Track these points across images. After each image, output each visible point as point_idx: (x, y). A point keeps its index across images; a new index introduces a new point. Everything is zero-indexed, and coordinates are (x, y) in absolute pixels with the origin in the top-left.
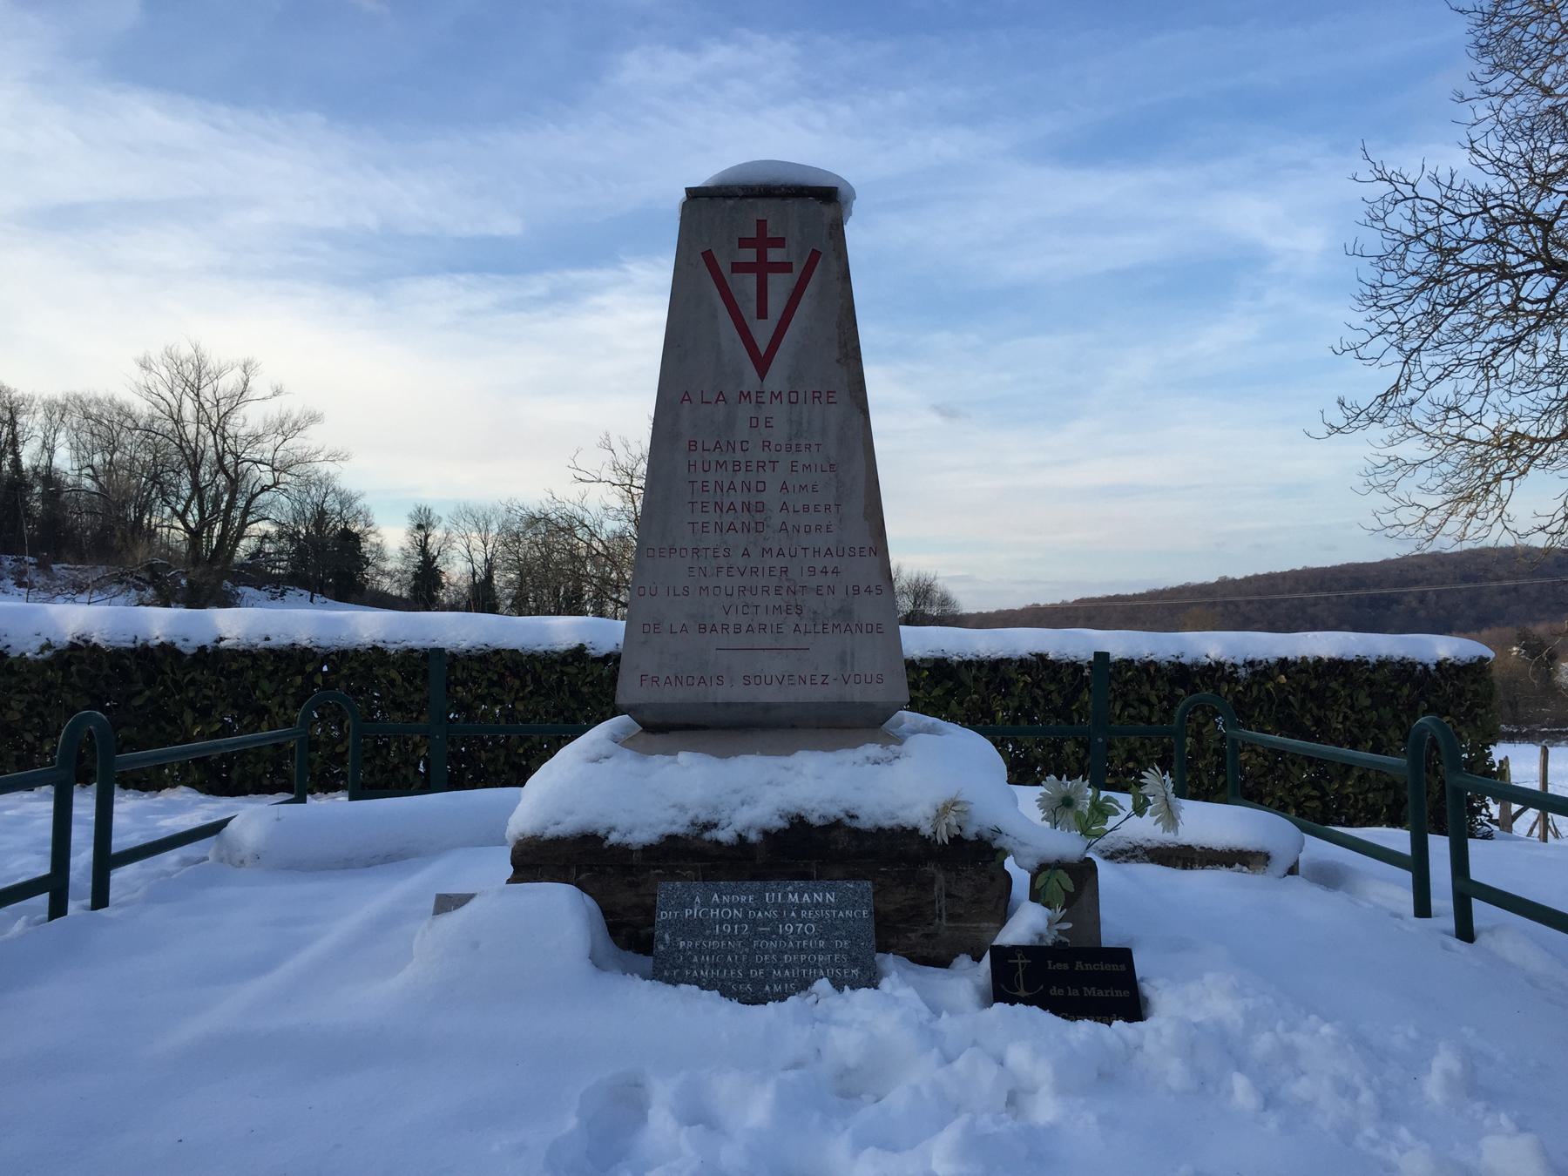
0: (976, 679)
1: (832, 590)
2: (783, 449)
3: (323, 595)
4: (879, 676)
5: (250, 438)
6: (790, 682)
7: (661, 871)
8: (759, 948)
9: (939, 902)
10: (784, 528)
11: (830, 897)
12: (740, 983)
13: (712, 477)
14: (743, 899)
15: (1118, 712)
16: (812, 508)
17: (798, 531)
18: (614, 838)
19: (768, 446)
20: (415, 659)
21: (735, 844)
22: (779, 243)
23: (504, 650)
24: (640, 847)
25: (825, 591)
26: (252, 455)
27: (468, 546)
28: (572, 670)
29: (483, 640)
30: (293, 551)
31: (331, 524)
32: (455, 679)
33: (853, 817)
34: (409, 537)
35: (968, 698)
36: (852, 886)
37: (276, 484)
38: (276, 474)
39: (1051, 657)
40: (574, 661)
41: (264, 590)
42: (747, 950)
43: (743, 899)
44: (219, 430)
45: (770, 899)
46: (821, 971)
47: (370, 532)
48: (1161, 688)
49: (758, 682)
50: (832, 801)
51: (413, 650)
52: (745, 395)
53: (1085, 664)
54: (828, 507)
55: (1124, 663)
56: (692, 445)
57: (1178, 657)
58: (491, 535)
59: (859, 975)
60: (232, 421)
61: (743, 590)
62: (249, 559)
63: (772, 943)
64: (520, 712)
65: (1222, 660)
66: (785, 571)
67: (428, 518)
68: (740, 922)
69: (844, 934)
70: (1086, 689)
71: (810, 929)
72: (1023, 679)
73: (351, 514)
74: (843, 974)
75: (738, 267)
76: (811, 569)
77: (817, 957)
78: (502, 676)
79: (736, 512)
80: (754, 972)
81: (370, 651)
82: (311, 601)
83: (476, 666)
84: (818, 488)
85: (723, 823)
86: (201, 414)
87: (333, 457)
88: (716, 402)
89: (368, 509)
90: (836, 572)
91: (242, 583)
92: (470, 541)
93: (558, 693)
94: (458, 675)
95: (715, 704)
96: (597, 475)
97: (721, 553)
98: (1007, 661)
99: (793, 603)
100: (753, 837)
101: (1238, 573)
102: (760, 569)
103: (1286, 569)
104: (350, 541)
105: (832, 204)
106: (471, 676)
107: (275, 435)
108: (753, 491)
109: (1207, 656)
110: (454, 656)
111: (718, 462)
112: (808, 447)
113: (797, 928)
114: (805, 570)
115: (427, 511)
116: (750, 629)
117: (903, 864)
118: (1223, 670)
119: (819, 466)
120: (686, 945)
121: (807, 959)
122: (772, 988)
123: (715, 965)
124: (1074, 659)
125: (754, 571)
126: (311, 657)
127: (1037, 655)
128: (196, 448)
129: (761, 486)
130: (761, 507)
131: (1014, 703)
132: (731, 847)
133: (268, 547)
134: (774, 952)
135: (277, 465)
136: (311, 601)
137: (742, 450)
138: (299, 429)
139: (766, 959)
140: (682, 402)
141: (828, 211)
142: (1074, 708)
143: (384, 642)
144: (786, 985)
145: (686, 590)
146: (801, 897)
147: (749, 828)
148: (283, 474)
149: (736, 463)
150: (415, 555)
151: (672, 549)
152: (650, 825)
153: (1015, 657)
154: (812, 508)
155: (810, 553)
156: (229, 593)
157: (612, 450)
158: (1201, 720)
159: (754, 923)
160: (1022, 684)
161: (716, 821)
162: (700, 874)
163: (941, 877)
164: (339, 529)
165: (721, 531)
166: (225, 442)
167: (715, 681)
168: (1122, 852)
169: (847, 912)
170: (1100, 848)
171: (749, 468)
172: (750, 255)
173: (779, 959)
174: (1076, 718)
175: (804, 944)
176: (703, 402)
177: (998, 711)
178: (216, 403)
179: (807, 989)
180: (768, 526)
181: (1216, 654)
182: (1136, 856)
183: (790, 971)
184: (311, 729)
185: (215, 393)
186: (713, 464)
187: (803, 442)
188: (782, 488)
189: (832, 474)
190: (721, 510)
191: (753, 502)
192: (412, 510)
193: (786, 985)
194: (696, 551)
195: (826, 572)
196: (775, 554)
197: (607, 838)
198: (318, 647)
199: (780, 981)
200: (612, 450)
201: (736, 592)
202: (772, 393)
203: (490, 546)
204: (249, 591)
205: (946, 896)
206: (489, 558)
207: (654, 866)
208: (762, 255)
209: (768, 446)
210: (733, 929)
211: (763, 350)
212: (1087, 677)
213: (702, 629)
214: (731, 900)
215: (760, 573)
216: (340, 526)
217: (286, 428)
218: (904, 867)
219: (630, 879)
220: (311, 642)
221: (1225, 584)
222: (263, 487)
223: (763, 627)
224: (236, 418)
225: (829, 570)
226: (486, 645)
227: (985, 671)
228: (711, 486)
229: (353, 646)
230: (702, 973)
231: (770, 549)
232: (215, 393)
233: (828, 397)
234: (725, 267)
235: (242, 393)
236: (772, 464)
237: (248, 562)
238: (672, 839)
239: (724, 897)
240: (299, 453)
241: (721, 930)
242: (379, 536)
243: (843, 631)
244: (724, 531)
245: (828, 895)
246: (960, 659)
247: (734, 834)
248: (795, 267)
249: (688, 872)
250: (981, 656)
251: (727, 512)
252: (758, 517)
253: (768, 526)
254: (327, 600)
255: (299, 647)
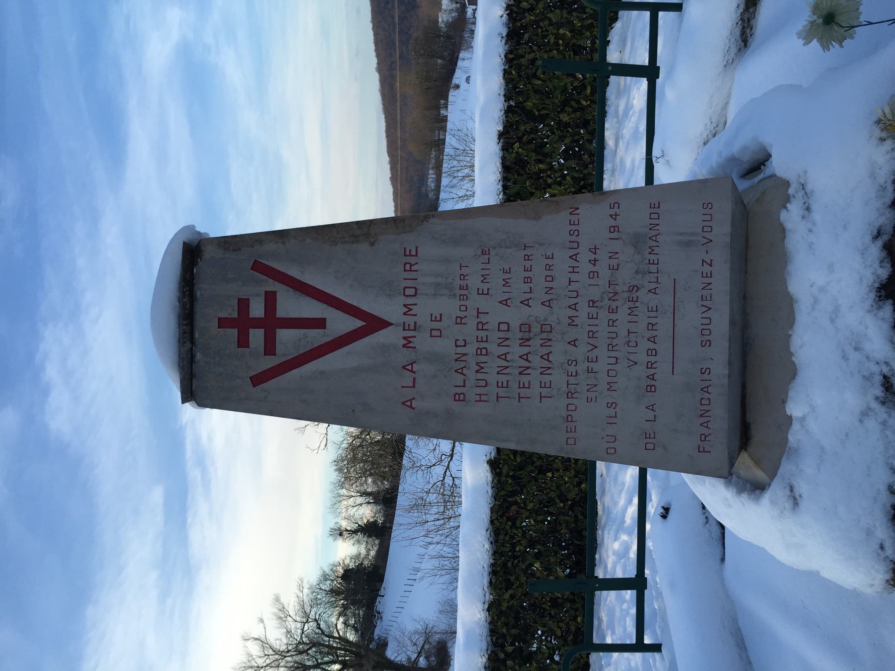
0: (515, 183)
1: (613, 255)
2: (463, 303)
3: (380, 589)
4: (705, 206)
5: (288, 636)
6: (708, 298)
10: (548, 304)
13: (493, 378)
15: (540, 82)
16: (527, 274)
17: (552, 288)
19: (461, 318)
20: (496, 581)
22: (244, 304)
23: (491, 518)
25: (614, 262)
26: (298, 634)
27: (353, 506)
28: (505, 470)
29: (484, 532)
30: (354, 607)
31: (339, 586)
32: (510, 552)
34: (347, 540)
35: (529, 188)
37: (316, 620)
38: (310, 620)
39: (501, 128)
40: (499, 468)
41: (376, 623)
44: (282, 654)
47: (344, 563)
48: (524, 50)
49: (707, 332)
50: (863, 253)
51: (491, 583)
52: (406, 342)
53: (506, 104)
54: (527, 258)
55: (506, 75)
56: (459, 398)
57: (502, 37)
58: (347, 494)
60: (278, 647)
61: (611, 347)
62: (358, 633)
64: (535, 506)
65: (505, 6)
66: (592, 303)
67: (336, 530)
70: (524, 104)
72: (516, 149)
73: (333, 574)
75: (270, 348)
76: (591, 276)
78: (509, 519)
79: (530, 353)
81: (491, 613)
82: (383, 596)
83: (501, 537)
84: (507, 268)
86: (273, 665)
87: (301, 588)
88: (414, 373)
89: (330, 564)
90: (594, 250)
91: (372, 636)
92: (350, 506)
93: (522, 478)
94: (508, 549)
95: (729, 376)
96: (322, 436)
97: (572, 369)
98: (503, 159)
99: (626, 295)
101: (374, 61)
102: (592, 328)
103: (371, 33)
104: (348, 574)
105: (203, 248)
106: (509, 541)
107: (287, 622)
108: (509, 335)
109: (502, 17)
110: (495, 553)
111: (477, 372)
112: (463, 277)
114: (592, 282)
115: (332, 530)
116: (651, 339)
118: (512, 5)
119: (484, 266)
124: (503, 112)
125: (592, 335)
126: (493, 655)
127: (499, 139)
128: (295, 667)
129: (504, 327)
130: (526, 327)
131: (534, 156)
133: (352, 622)
135: (305, 620)
136: (383, 596)
137: (465, 346)
138: (284, 608)
140: (413, 408)
141: (209, 253)
142: (537, 113)
143: (484, 603)
145: (611, 405)
148: (310, 616)
149: (479, 353)
150: (357, 537)
151: (568, 419)
153: (501, 154)
154: (527, 274)
155: (574, 277)
156: (378, 644)
157: (306, 426)
158: (547, 22)
160: (520, 150)
164: (341, 581)
165: (550, 368)
166: (290, 651)
167: (705, 376)
168: (743, 33)
170: (736, 51)
171: (484, 339)
172: (257, 336)
174: (544, 112)
176: (414, 387)
177: (538, 167)
178: (267, 657)
180: (546, 320)
181: (501, 10)
182: (748, 19)
184: (544, 654)
185: (260, 657)
186: (480, 376)
187: (458, 282)
188: (506, 305)
189: (493, 252)
190: (528, 368)
191: (520, 335)
192: (331, 539)
194: (570, 394)
195: (595, 260)
196: (576, 314)
198: (487, 650)
200: (306, 426)
201: (613, 354)
202: (405, 314)
203: (353, 494)
204: (377, 632)
206: (360, 495)
208: (257, 323)
209: (461, 318)
211: (359, 323)
212: (515, 103)
213: (651, 388)
215: (594, 329)
216: (340, 580)
217: (282, 615)
220: (484, 655)
221: (380, 69)
222: (318, 628)
223: (651, 326)
224: (276, 645)
225: (593, 257)
226: (487, 530)
227: (510, 176)
228: (503, 379)
229: (487, 625)
231: (569, 317)
232: (260, 657)
233: (410, 255)
234: (270, 362)
235: (261, 641)
236: (480, 315)
237: (360, 633)
240: (297, 608)
242: (346, 558)
243: (656, 244)
244: (550, 366)
246: (502, 193)
248: (271, 288)
250: (499, 178)
251: (529, 362)
252: (536, 329)
253: (546, 320)
254: (383, 587)
255: (487, 664)
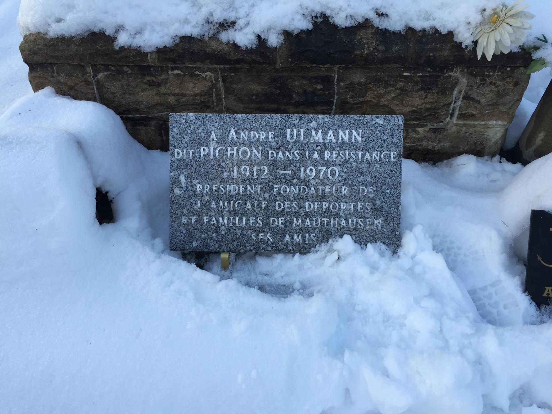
7: (179, 72)
8: (279, 193)
9: (454, 104)
11: (357, 136)
12: (260, 232)
14: (263, 136)
18: (123, 40)
21: (254, 47)
24: (153, 49)
33: (381, 15)
36: (381, 122)
42: (267, 196)
43: (263, 136)
45: (292, 136)
46: (343, 221)
59: (382, 226)
63: (293, 188)
68: (259, 164)
69: (369, 179)
71: (333, 174)
74: (365, 224)
77: (340, 205)
80: (274, 221)
85: (241, 23)
100: (274, 40)
113: (320, 172)
117: (429, 69)
120: (203, 189)
121: (329, 207)
122: (292, 237)
123: (235, 211)
132: (249, 51)
134: (295, 198)
139: (286, 206)
144: (307, 235)
146: (325, 134)
147: (269, 29)
152: (161, 24)
159: (274, 164)
161: (233, 19)
162: (220, 75)
163: (464, 81)
169: (374, 154)
173: (300, 207)
175: (327, 190)
179: (328, 241)
183: (311, 220)
193: (307, 235)
197: (115, 38)
199: (301, 230)
205: (464, 98)
207: (172, 67)
210: (252, 172)
214: (249, 137)
218: (429, 72)
219: (149, 78)
230: (221, 220)
238: (186, 39)
239: (242, 134)
241: (239, 173)
245: (354, 133)
247: (253, 38)
249: (207, 73)
